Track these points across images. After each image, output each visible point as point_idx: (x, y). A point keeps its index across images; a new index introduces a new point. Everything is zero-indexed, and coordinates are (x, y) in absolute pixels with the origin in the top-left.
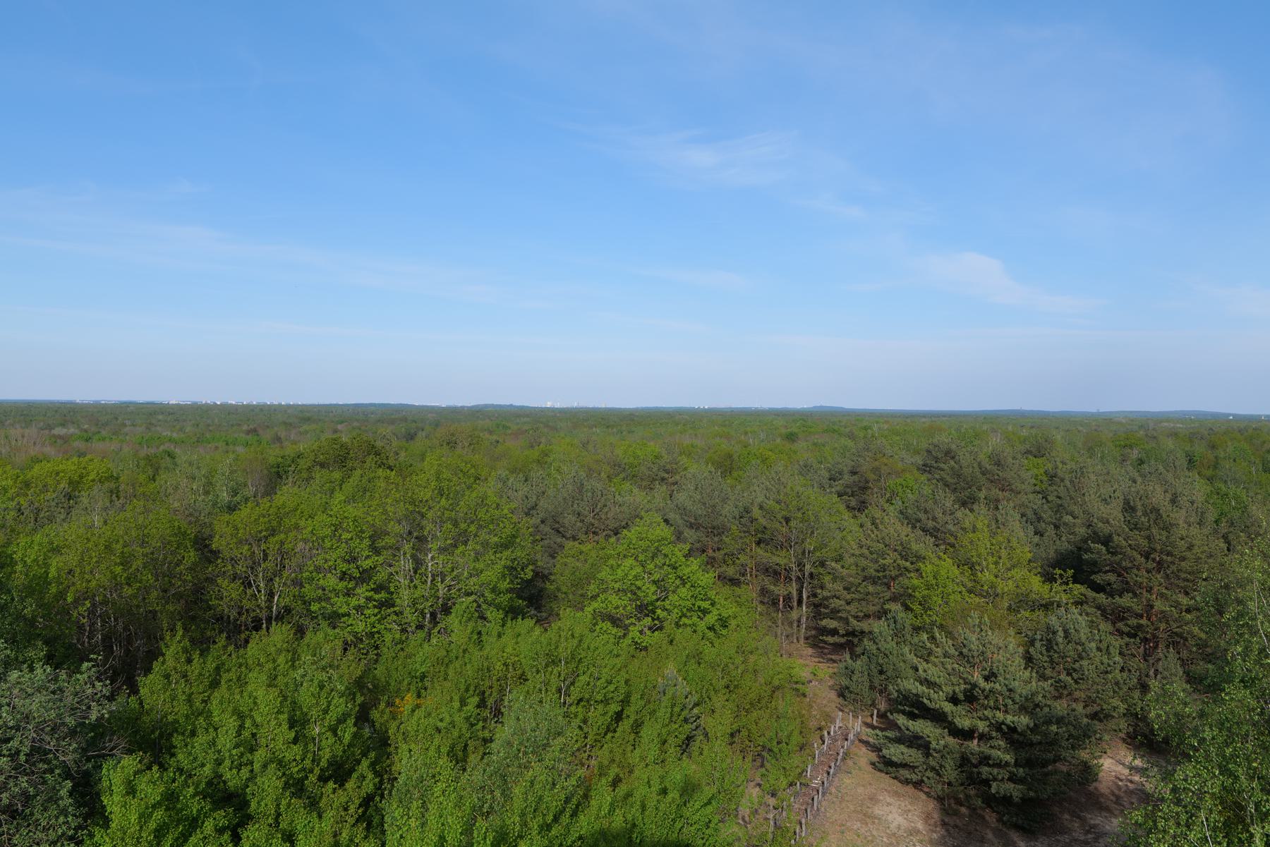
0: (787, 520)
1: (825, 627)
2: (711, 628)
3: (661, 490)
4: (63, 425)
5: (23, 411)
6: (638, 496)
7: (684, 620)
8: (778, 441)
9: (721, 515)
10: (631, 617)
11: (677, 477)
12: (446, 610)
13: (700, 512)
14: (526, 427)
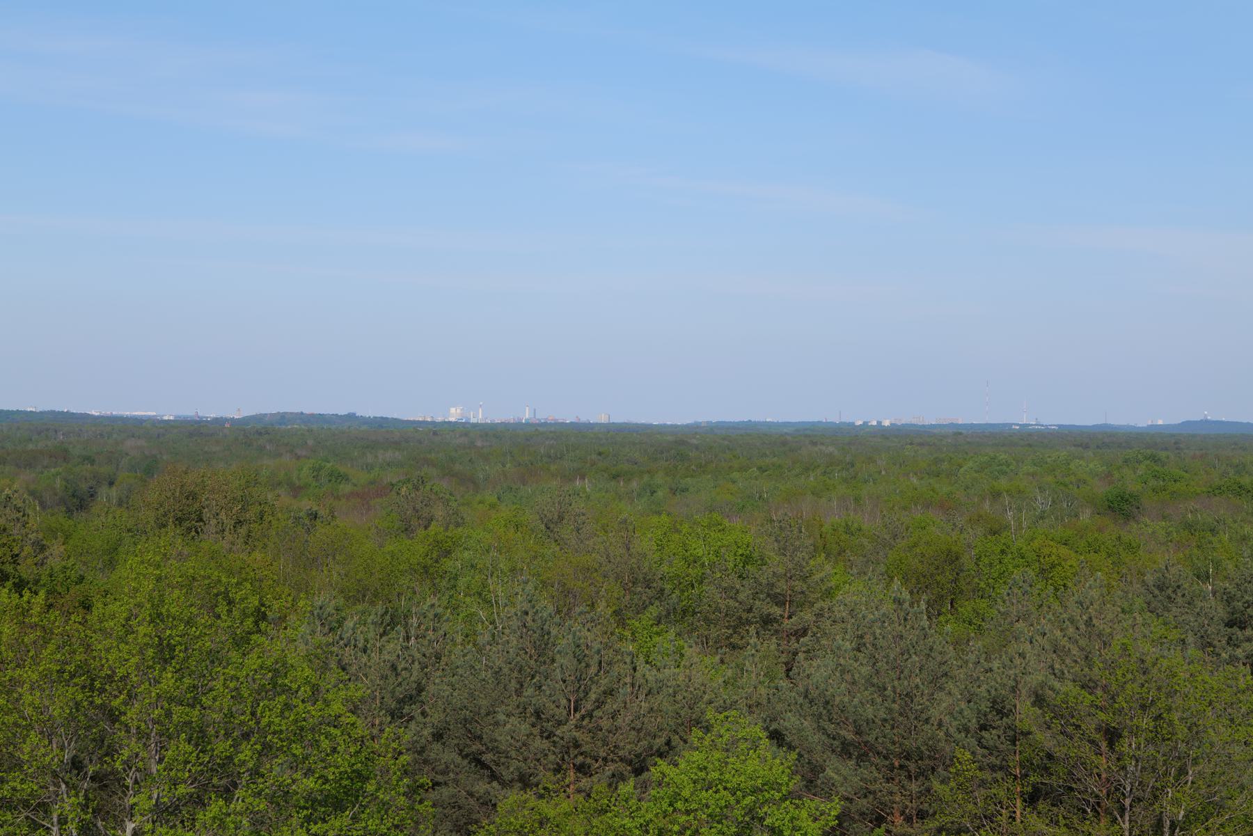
0: (1112, 736)
8: (1085, 517)
11: (807, 616)
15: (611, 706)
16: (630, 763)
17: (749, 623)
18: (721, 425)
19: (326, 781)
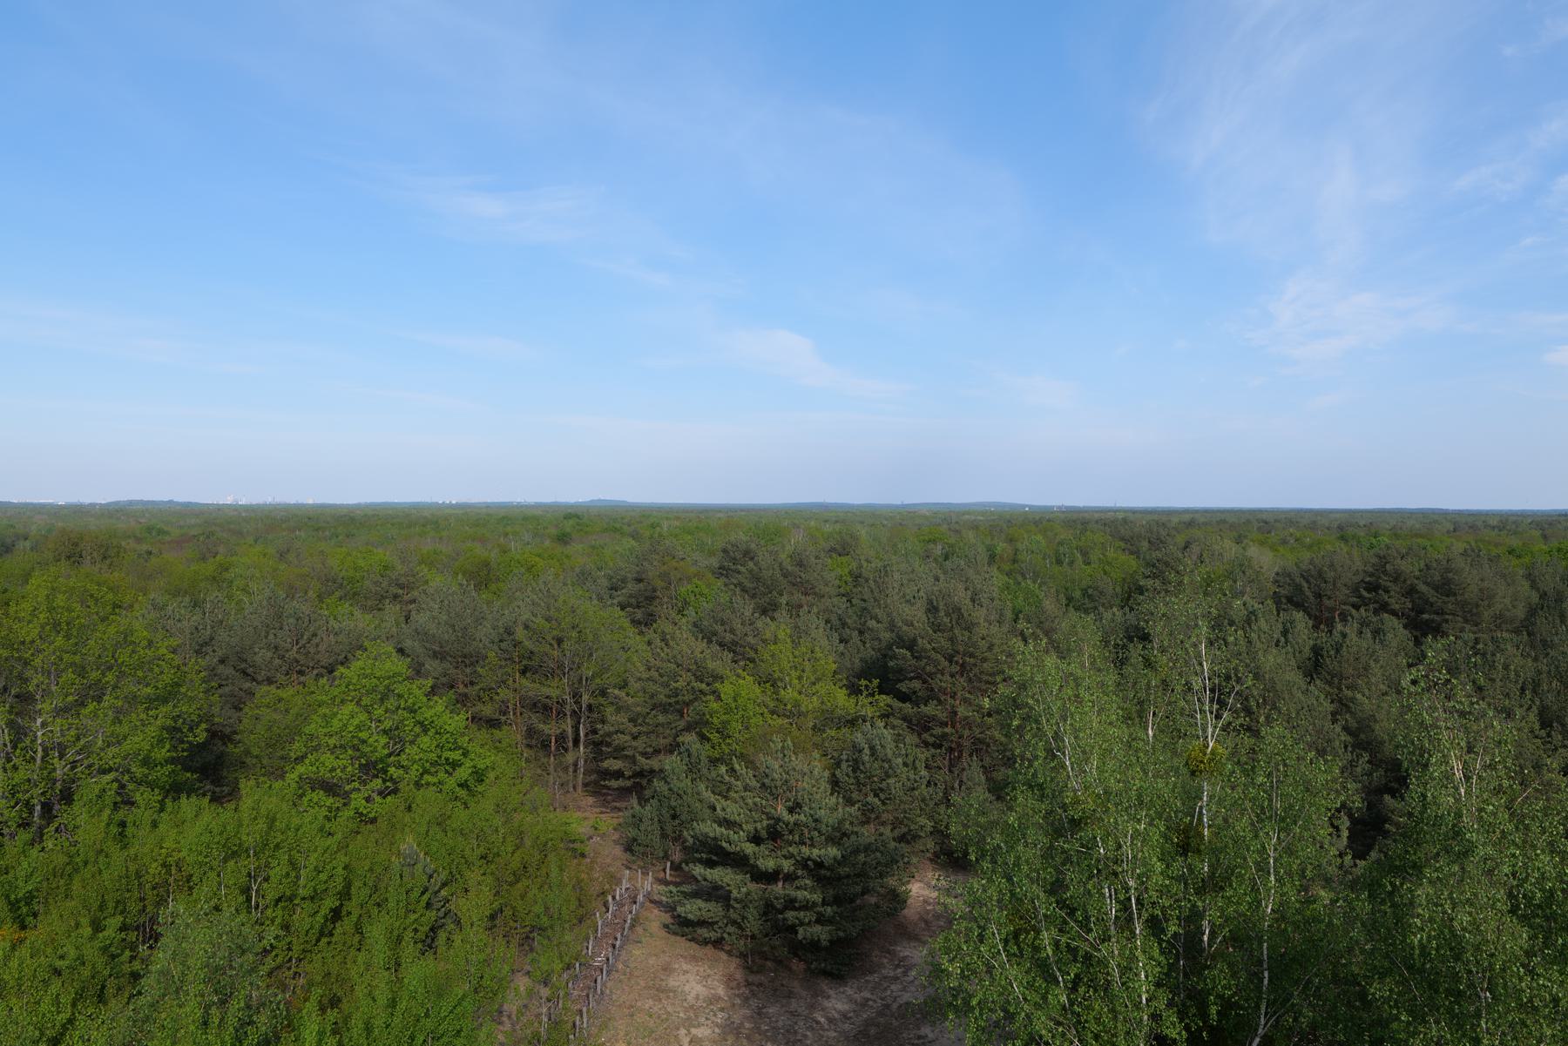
0: (560, 641)
1: (607, 770)
2: (463, 785)
3: (392, 611)
6: (362, 621)
7: (427, 778)
8: (547, 543)
9: (474, 640)
10: (354, 781)
11: (416, 593)
12: (67, 797)
13: (446, 637)
14: (194, 532)
15: (315, 640)
16: (326, 668)
17: (387, 597)
18: (368, 506)
19: (157, 688)
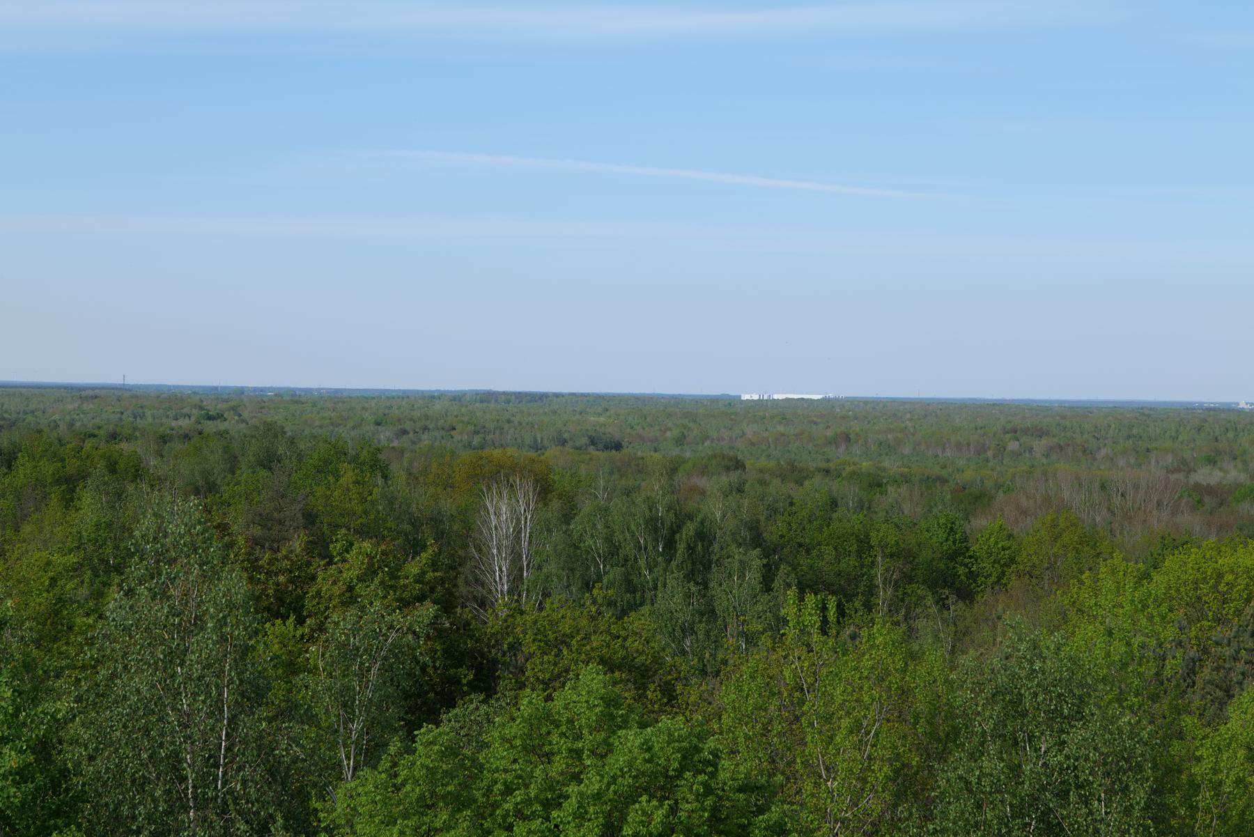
4: (1212, 462)
5: (1131, 427)
